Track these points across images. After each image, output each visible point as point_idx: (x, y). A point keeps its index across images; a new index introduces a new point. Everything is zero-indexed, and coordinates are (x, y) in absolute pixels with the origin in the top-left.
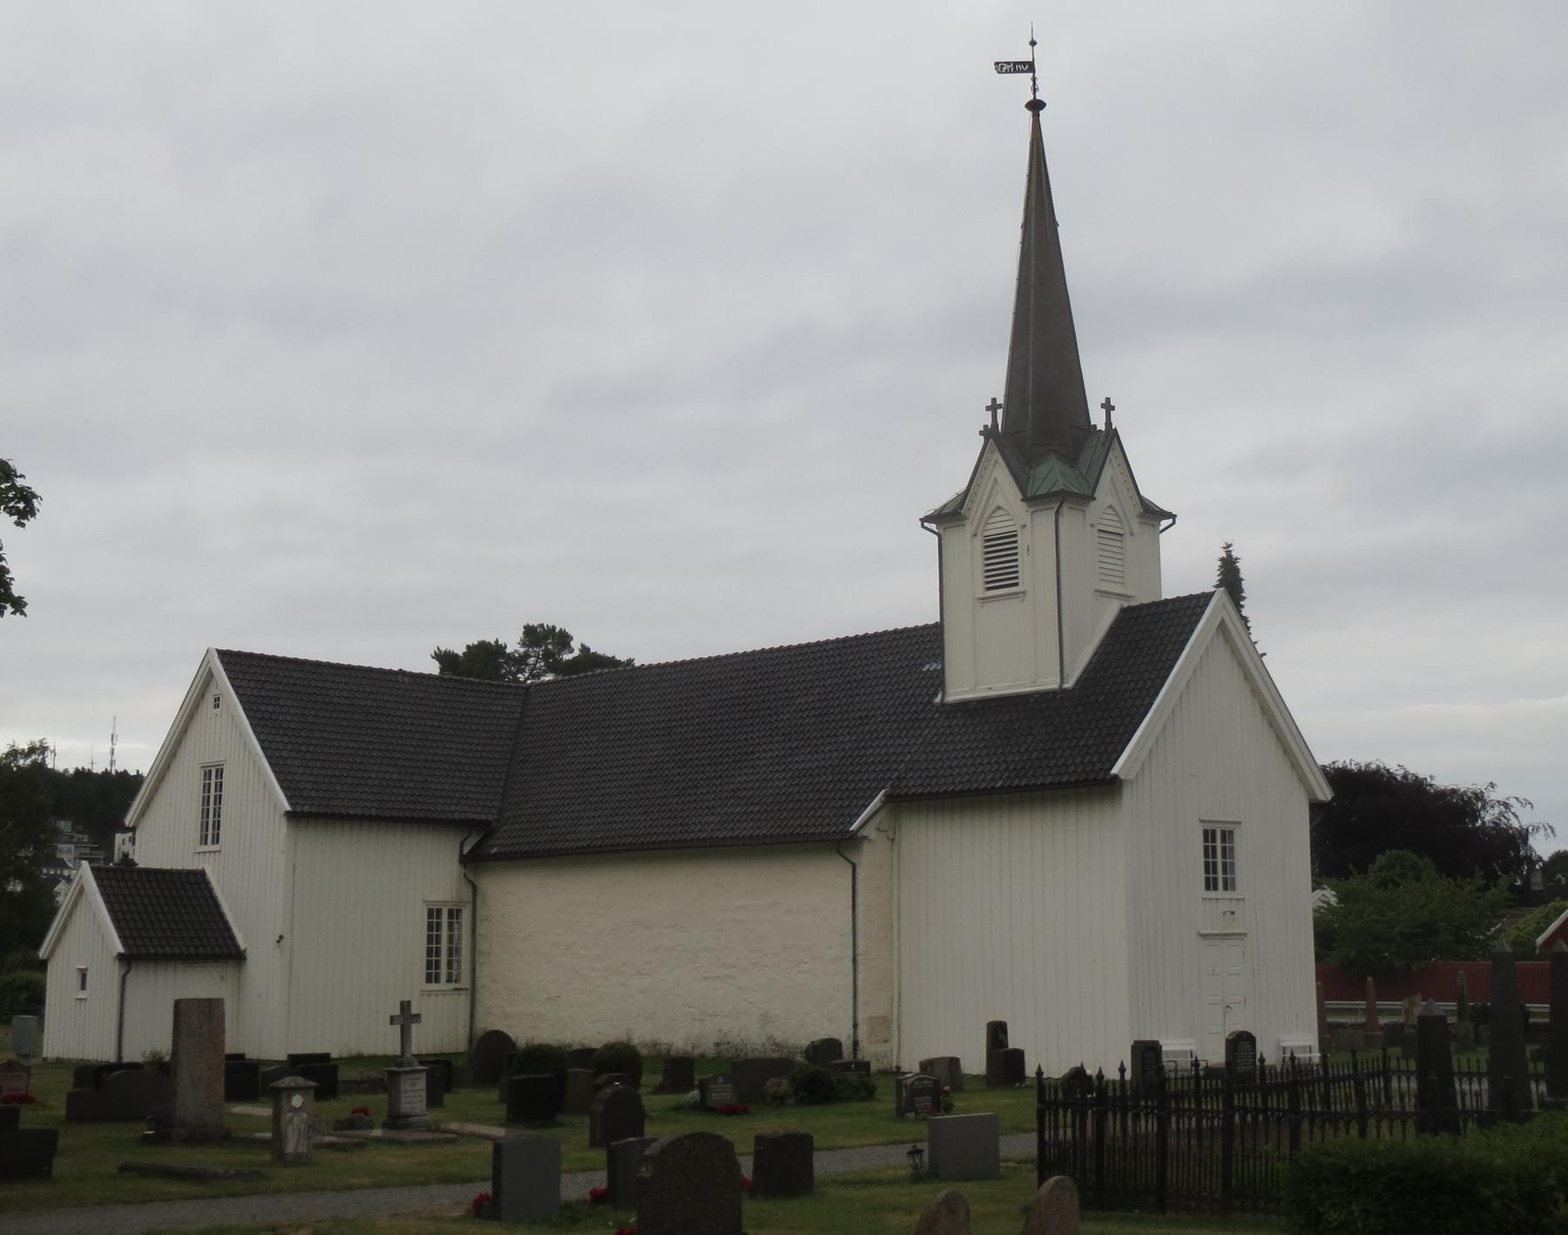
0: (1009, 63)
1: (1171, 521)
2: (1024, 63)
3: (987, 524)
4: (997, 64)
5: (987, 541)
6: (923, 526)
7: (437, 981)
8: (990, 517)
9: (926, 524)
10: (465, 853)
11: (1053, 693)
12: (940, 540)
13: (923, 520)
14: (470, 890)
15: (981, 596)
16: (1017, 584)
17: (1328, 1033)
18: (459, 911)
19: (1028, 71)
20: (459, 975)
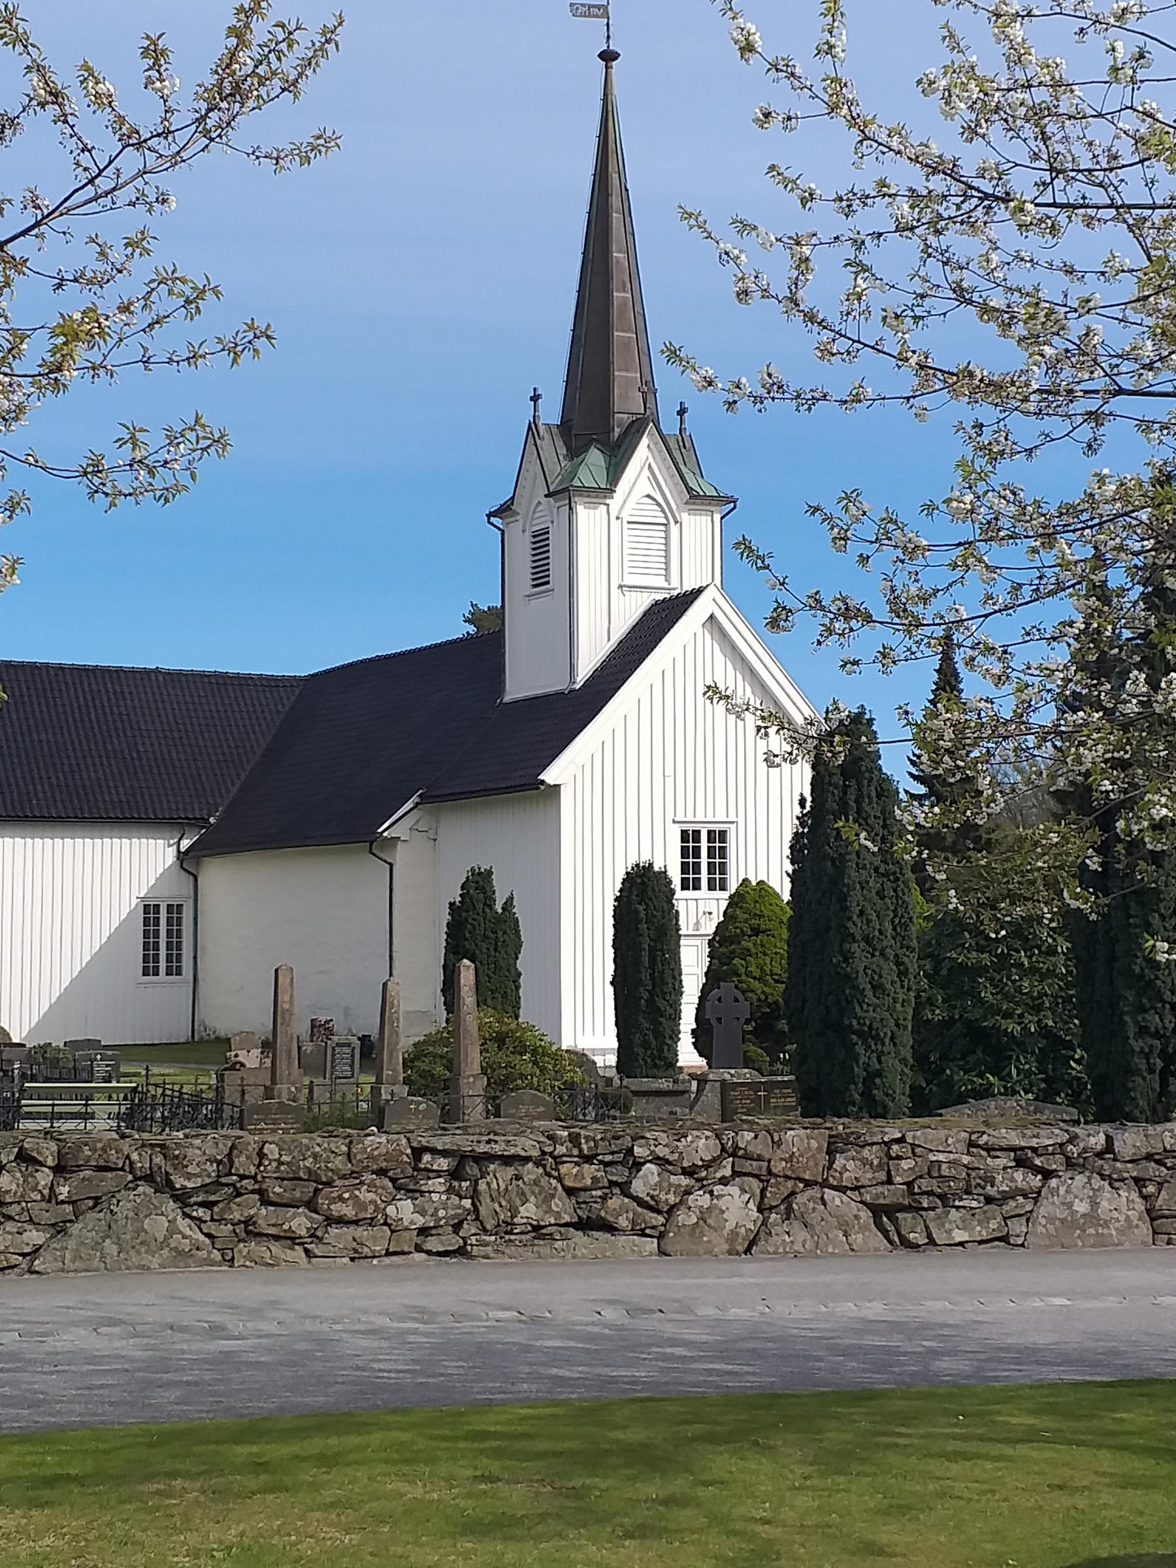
0: (583, 5)
1: (732, 505)
2: (599, 7)
3: (533, 519)
4: (571, 5)
5: (534, 537)
6: (489, 522)
7: (156, 974)
8: (534, 512)
9: (492, 520)
10: (182, 850)
11: (559, 694)
12: (503, 535)
13: (489, 516)
14: (192, 878)
15: (527, 593)
16: (548, 583)
17: (681, 1068)
18: (180, 906)
19: (602, 17)
20: (179, 968)
